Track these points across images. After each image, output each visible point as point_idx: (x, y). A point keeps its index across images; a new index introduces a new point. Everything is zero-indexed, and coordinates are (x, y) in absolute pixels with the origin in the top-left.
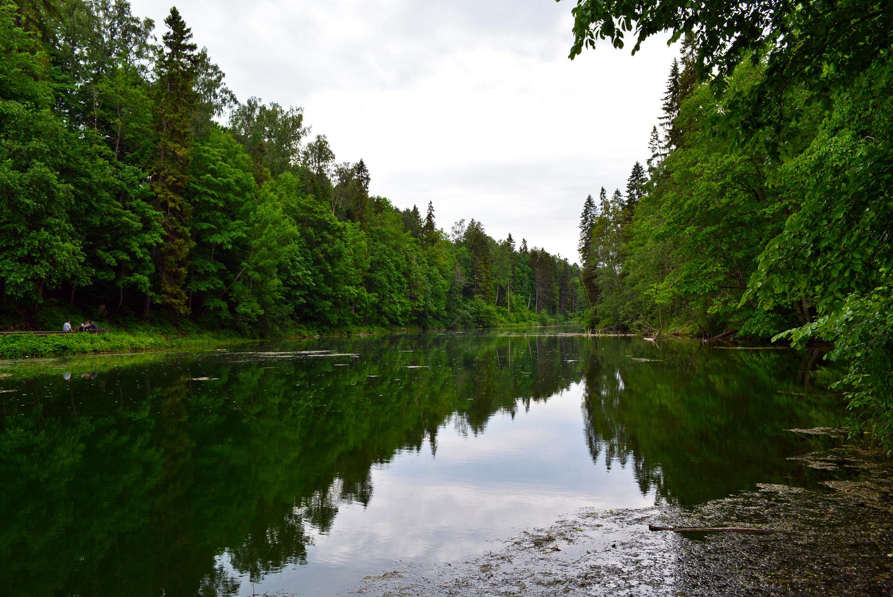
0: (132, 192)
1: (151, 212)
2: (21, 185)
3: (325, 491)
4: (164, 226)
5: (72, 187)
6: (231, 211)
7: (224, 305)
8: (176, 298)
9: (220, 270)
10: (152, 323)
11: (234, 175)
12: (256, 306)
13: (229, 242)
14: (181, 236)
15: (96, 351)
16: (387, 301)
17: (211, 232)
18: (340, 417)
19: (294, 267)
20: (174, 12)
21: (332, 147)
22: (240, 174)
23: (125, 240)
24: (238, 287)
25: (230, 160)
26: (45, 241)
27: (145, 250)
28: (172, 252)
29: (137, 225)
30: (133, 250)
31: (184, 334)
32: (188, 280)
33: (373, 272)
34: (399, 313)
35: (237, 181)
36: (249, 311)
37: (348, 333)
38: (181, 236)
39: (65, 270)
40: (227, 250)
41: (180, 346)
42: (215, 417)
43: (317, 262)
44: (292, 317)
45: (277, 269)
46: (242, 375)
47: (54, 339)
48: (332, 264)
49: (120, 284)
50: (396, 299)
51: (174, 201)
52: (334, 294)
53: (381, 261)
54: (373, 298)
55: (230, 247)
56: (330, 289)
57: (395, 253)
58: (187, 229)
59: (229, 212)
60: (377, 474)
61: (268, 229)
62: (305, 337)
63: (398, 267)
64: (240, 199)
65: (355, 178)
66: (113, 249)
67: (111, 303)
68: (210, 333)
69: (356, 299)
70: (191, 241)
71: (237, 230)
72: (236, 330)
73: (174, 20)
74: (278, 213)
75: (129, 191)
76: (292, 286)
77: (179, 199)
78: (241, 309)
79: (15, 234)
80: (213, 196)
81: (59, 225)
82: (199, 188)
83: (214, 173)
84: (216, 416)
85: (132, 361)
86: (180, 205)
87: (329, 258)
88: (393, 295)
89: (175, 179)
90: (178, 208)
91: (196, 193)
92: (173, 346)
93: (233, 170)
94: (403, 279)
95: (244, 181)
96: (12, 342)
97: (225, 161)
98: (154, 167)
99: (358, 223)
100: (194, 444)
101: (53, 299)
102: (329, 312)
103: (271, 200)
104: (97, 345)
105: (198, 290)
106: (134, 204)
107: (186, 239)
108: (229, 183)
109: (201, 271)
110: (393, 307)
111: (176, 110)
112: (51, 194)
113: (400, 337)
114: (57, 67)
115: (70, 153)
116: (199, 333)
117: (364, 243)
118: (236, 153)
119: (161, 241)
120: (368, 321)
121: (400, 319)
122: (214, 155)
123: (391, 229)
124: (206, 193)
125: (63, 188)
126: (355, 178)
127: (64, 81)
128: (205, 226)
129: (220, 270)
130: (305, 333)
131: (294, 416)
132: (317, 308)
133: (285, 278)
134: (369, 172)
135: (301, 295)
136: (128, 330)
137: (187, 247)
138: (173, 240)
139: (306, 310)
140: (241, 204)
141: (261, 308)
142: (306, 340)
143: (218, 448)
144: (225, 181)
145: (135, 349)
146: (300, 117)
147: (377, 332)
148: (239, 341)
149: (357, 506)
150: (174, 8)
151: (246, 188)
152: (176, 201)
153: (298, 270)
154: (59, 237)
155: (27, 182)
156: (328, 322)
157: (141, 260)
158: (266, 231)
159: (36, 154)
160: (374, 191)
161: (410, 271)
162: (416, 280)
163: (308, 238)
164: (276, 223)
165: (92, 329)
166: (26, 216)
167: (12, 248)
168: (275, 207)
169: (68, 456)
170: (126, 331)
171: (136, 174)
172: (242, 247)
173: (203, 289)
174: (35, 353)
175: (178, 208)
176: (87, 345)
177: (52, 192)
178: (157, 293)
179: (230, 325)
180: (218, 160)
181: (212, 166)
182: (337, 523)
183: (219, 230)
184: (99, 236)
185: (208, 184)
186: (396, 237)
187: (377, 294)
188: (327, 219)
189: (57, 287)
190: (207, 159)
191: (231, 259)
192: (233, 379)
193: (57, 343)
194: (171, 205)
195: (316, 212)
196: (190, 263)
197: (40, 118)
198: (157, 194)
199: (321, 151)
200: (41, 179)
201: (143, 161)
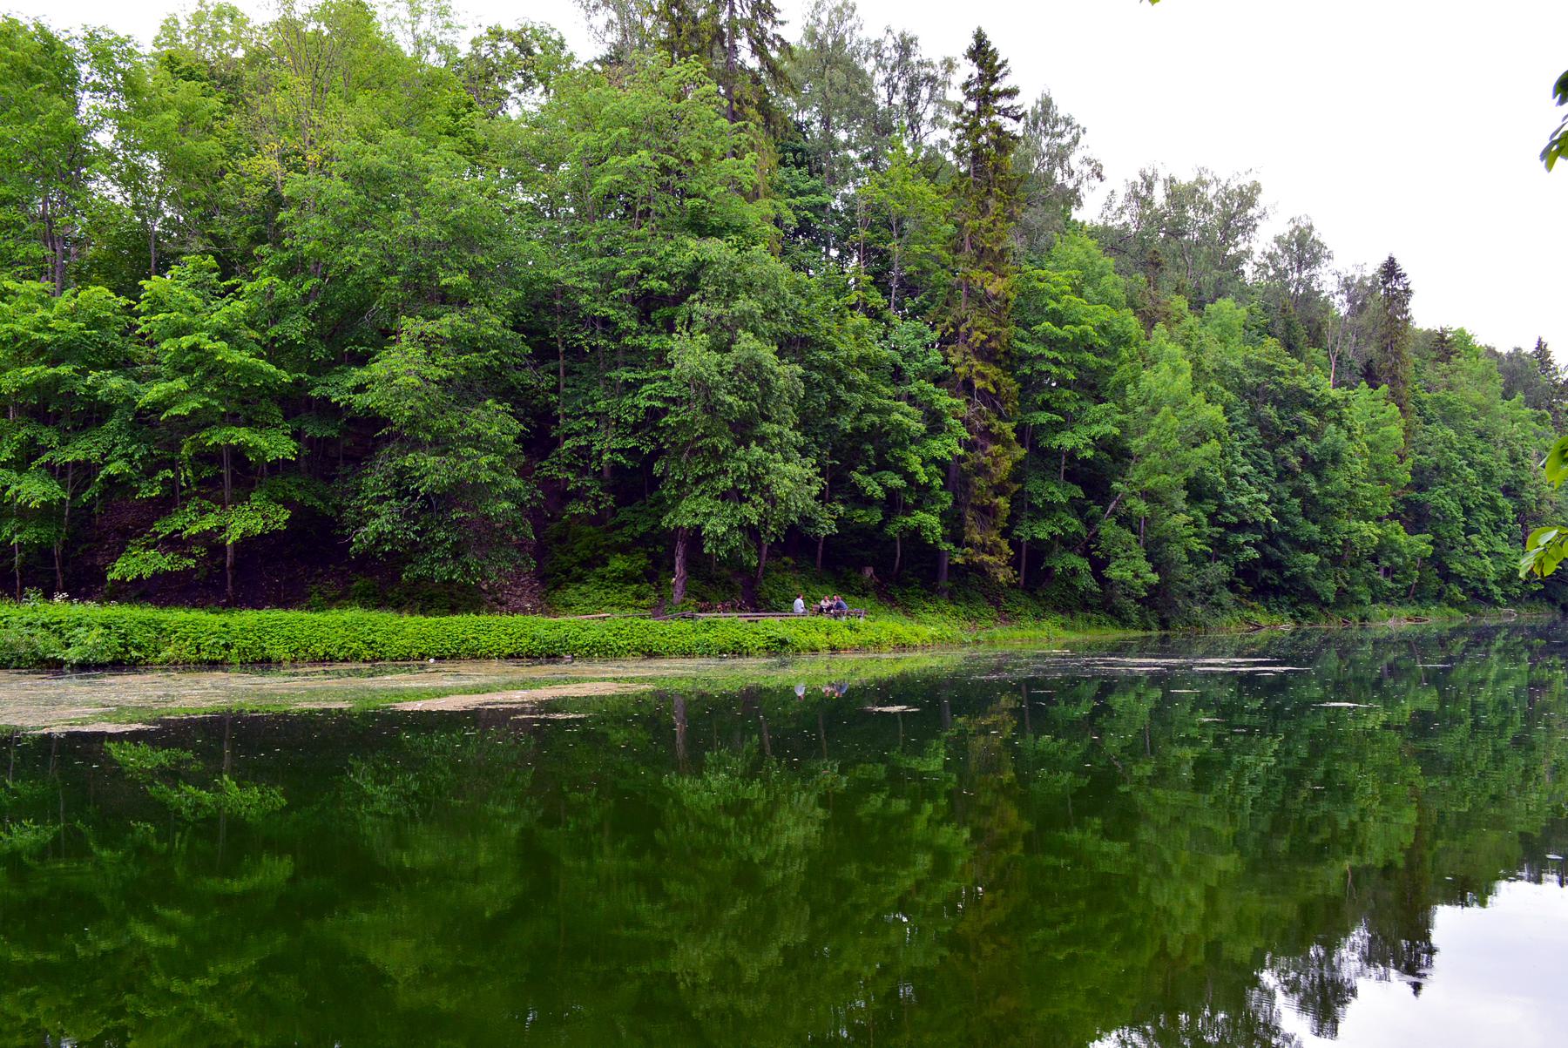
0: (911, 369)
1: (942, 399)
2: (721, 373)
3: (1331, 946)
4: (966, 422)
5: (799, 370)
6: (1093, 387)
7: (1083, 564)
8: (991, 554)
9: (1072, 499)
10: (952, 599)
11: (1091, 315)
12: (1144, 567)
13: (1087, 446)
14: (995, 439)
15: (833, 649)
16: (1460, 551)
17: (1057, 428)
18: (1346, 793)
19: (1232, 486)
20: (980, 38)
21: (1322, 233)
22: (1105, 314)
23: (898, 452)
24: (1108, 528)
25: (1088, 290)
26: (759, 463)
27: (933, 468)
28: (981, 470)
29: (917, 427)
30: (910, 470)
31: (1007, 617)
32: (1013, 519)
33: (1426, 490)
34: (1493, 577)
35: (1103, 329)
36: (1129, 575)
37: (1363, 619)
38: (995, 439)
39: (788, 509)
40: (1085, 461)
41: (992, 642)
42: (1066, 778)
43: (1286, 473)
44: (1232, 586)
45: (1185, 494)
46: (1117, 701)
47: (773, 625)
48: (1318, 477)
49: (891, 530)
50: (1481, 546)
51: (983, 376)
52: (1326, 538)
53: (1443, 464)
54: (1421, 544)
55: (1089, 454)
56: (1317, 528)
57: (1480, 445)
58: (1008, 428)
59: (1093, 387)
60: (1449, 923)
61: (1161, 414)
62: (1260, 627)
63: (1487, 476)
64: (1107, 362)
65: (1387, 289)
66: (878, 469)
67: (875, 562)
68: (1059, 617)
69: (1380, 549)
70: (1017, 447)
71: (1102, 422)
72: (1111, 612)
73: (981, 52)
74: (1183, 381)
75: (905, 365)
76: (1227, 527)
77: (992, 371)
78: (1114, 572)
79: (716, 455)
80: (1056, 362)
81: (780, 435)
82: (1029, 348)
83: (1058, 319)
84: (1069, 774)
85: (899, 668)
86: (995, 384)
87: (1314, 466)
88: (1474, 537)
89: (984, 337)
90: (992, 390)
91: (1024, 358)
92: (978, 642)
93: (1091, 308)
94: (1503, 502)
95: (1117, 326)
96: (706, 631)
97: (1079, 292)
98: (949, 319)
99: (1384, 388)
100: (1027, 826)
101: (786, 559)
102: (1315, 577)
103: (1171, 358)
104: (836, 639)
105: (1033, 537)
106: (913, 389)
107: (1007, 444)
108: (1085, 335)
109: (1038, 502)
110: (1475, 563)
111: (984, 211)
112: (765, 384)
113: (1497, 629)
114: (802, 169)
115: (804, 311)
116: (1038, 617)
117: (1395, 431)
118: (1102, 275)
119: (961, 451)
120: (1415, 595)
121: (1497, 590)
122: (1057, 285)
123: (1469, 394)
124: (1041, 356)
125: (787, 374)
126: (1387, 289)
127: (813, 191)
128: (1043, 417)
129: (1072, 499)
130: (1261, 619)
131: (1237, 788)
132: (1288, 568)
133: (1213, 509)
134: (1409, 278)
135: (1247, 543)
136: (908, 611)
137: (1005, 459)
138: (983, 448)
139: (1265, 573)
140: (1110, 370)
141: (1154, 571)
142: (1263, 633)
143: (1075, 835)
144: (1077, 330)
145: (903, 647)
146: (1256, 188)
147: (1437, 619)
148: (1114, 634)
149: (1399, 983)
150: (979, 30)
151: (1122, 340)
152: (988, 375)
153: (1241, 492)
154: (778, 456)
155: (730, 368)
156: (1314, 597)
157: (927, 487)
158: (1157, 420)
159: (743, 321)
160: (1425, 315)
161: (1523, 483)
162: (1539, 502)
163: (1265, 427)
164: (1178, 403)
165: (836, 610)
166: (730, 422)
167: (712, 476)
168: (1177, 371)
169: (799, 826)
170: (905, 613)
171: (919, 335)
172: (1116, 452)
173: (1042, 535)
174: (739, 651)
175: (992, 390)
176: (819, 639)
177: (768, 381)
178: (957, 546)
179: (1103, 603)
180: (1064, 293)
181: (1053, 305)
182: (1352, 1015)
183: (1069, 421)
184: (847, 453)
185: (1051, 343)
186: (1484, 410)
187: (1430, 537)
188: (1305, 385)
189: (778, 539)
190: (1044, 292)
191: (1094, 477)
192: (1103, 710)
193: (771, 633)
194: (978, 383)
195: (1281, 374)
196: (1016, 487)
197: (750, 261)
198: (954, 366)
199: (1304, 248)
200: (750, 359)
201: (933, 310)
